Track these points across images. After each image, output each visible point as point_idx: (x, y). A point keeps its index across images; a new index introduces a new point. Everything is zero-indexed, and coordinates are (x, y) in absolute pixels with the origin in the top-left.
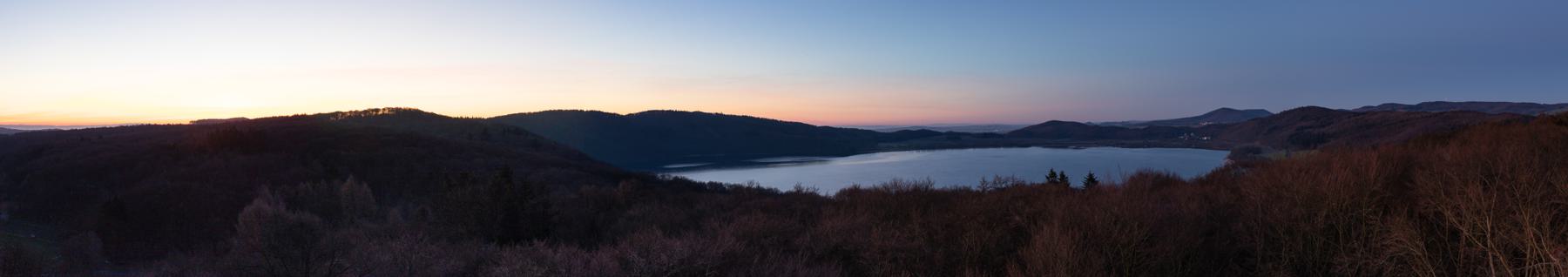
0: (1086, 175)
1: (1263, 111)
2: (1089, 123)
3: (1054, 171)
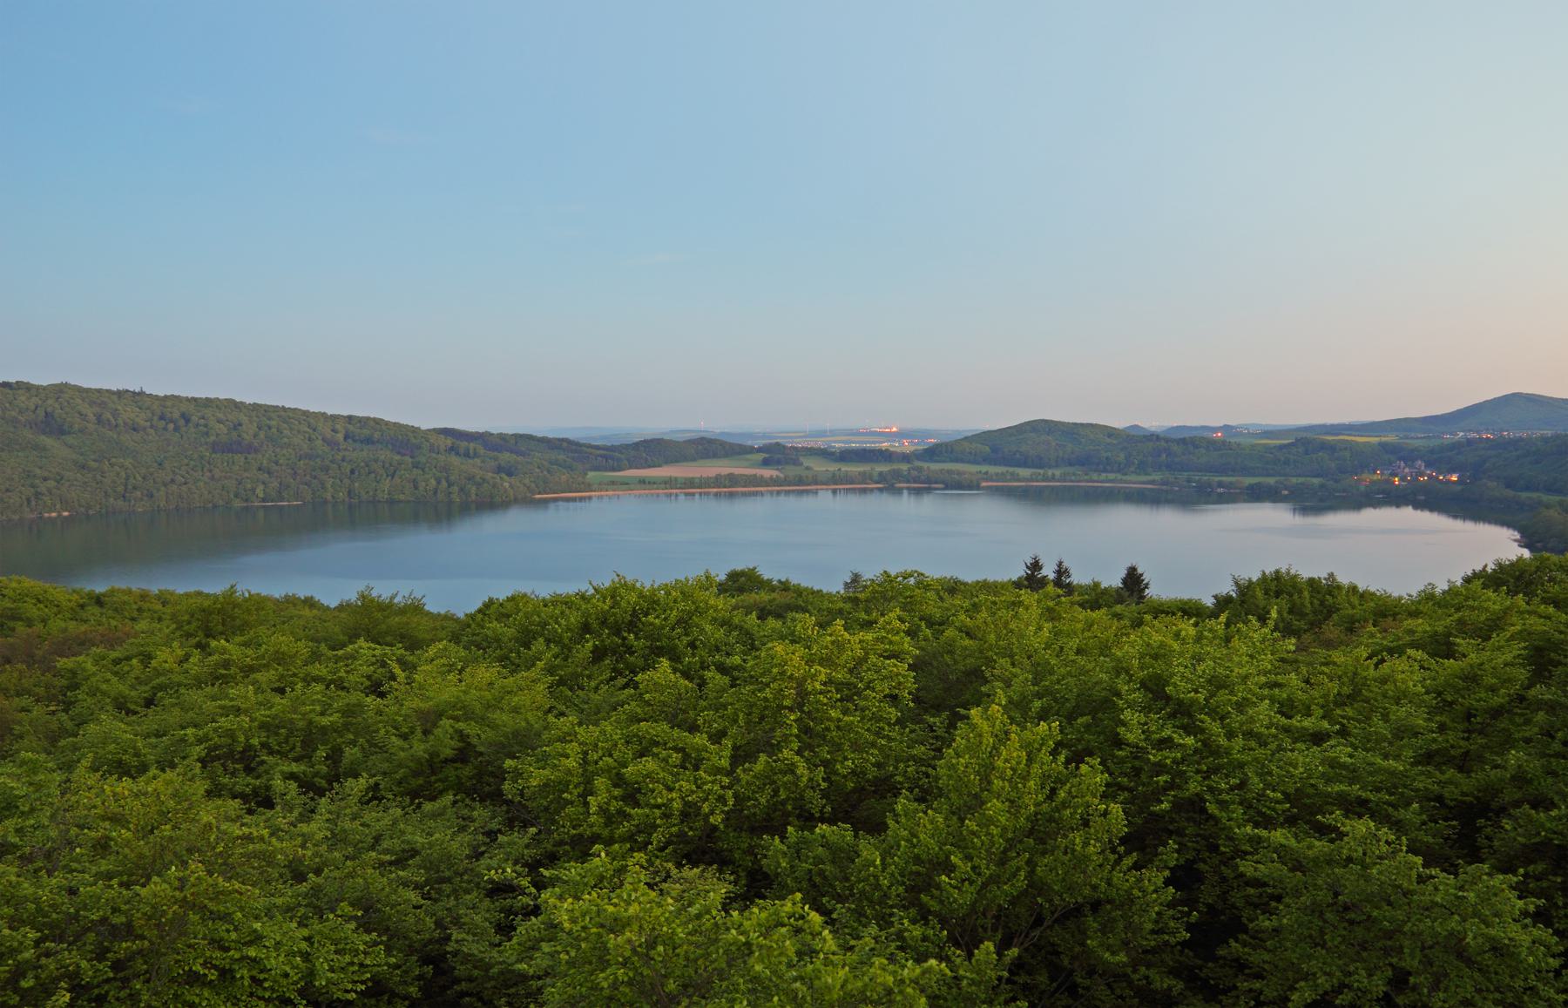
0: (1123, 573)
2: (1136, 427)
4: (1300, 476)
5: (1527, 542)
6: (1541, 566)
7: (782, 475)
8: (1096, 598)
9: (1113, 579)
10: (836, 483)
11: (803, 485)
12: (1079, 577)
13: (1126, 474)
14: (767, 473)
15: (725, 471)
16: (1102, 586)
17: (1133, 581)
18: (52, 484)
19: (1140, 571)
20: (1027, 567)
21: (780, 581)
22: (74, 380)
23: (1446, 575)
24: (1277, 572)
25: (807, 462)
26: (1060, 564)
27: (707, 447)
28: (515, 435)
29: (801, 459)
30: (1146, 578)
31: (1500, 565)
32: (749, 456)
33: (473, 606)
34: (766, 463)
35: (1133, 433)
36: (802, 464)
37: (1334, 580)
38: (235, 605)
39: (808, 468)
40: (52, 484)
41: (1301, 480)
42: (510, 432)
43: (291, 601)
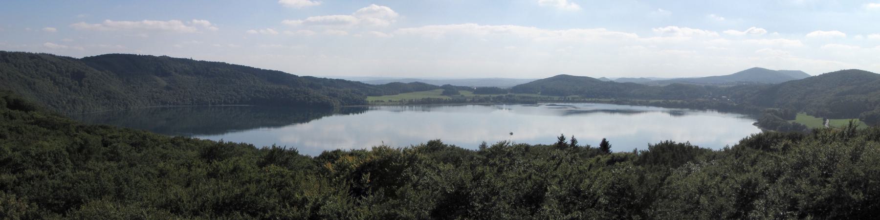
0: (600, 141)
1: (800, 72)
2: (604, 78)
3: (412, 144)
4: (673, 99)
5: (759, 124)
6: (767, 134)
7: (451, 99)
8: (589, 152)
9: (596, 145)
10: (474, 102)
11: (460, 102)
12: (581, 143)
13: (600, 98)
14: (445, 98)
15: (426, 97)
16: (591, 147)
17: (605, 145)
18: (158, 94)
19: (607, 140)
20: (559, 138)
21: (450, 145)
22: (168, 55)
23: (733, 141)
24: (667, 141)
25: (462, 93)
26: (573, 137)
27: (419, 86)
28: (337, 80)
29: (460, 91)
30: (610, 143)
31: (752, 136)
32: (436, 90)
33: (318, 154)
34: (444, 94)
35: (603, 80)
36: (459, 94)
37: (689, 144)
38: (222, 146)
39: (462, 96)
40: (158, 94)
41: (673, 101)
42: (335, 78)
43: (243, 145)
